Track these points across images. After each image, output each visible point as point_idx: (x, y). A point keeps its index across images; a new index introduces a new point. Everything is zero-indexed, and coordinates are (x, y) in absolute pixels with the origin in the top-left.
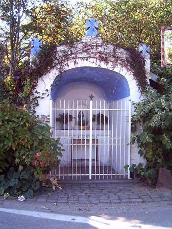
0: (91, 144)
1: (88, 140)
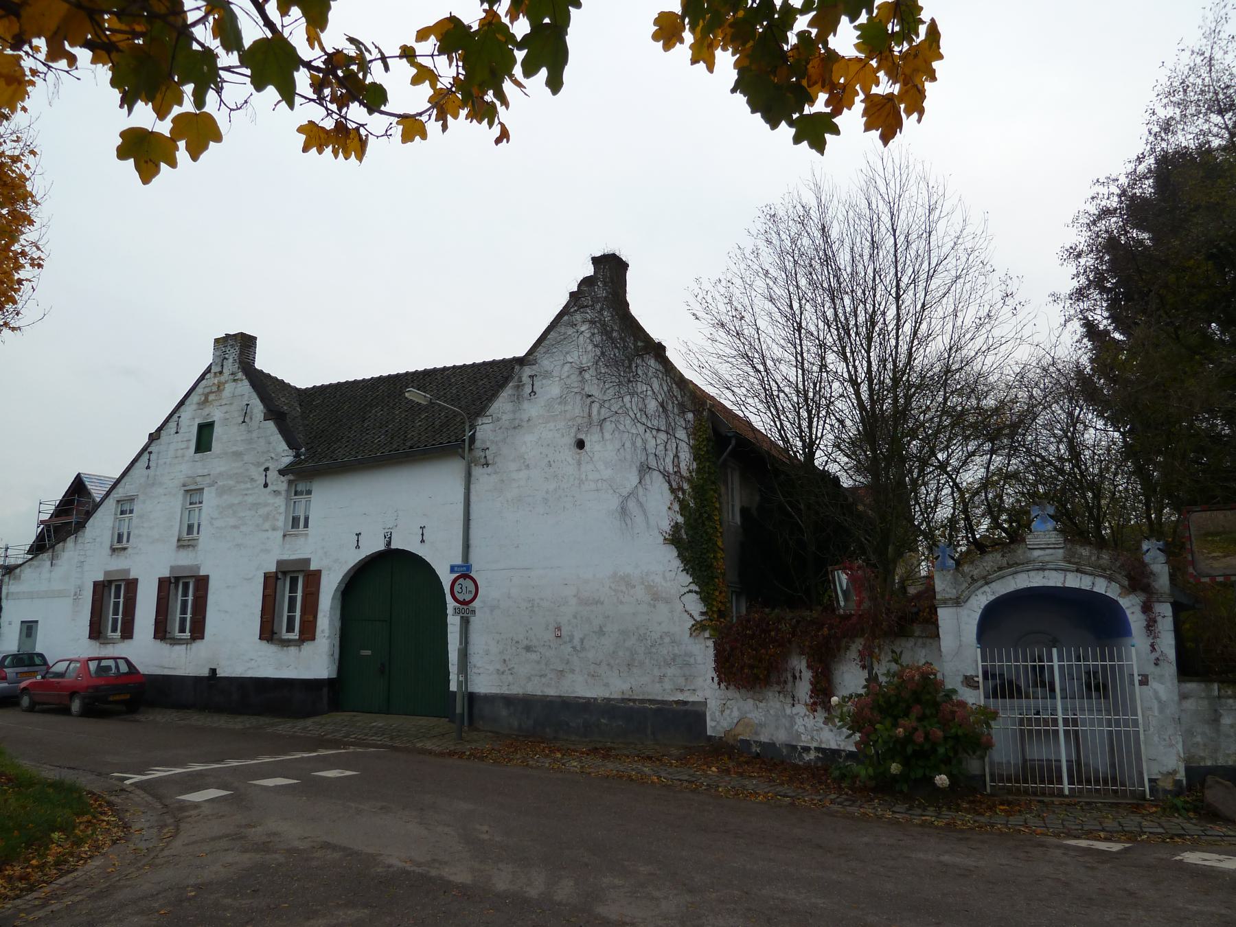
0: (1061, 728)
1: (1055, 722)
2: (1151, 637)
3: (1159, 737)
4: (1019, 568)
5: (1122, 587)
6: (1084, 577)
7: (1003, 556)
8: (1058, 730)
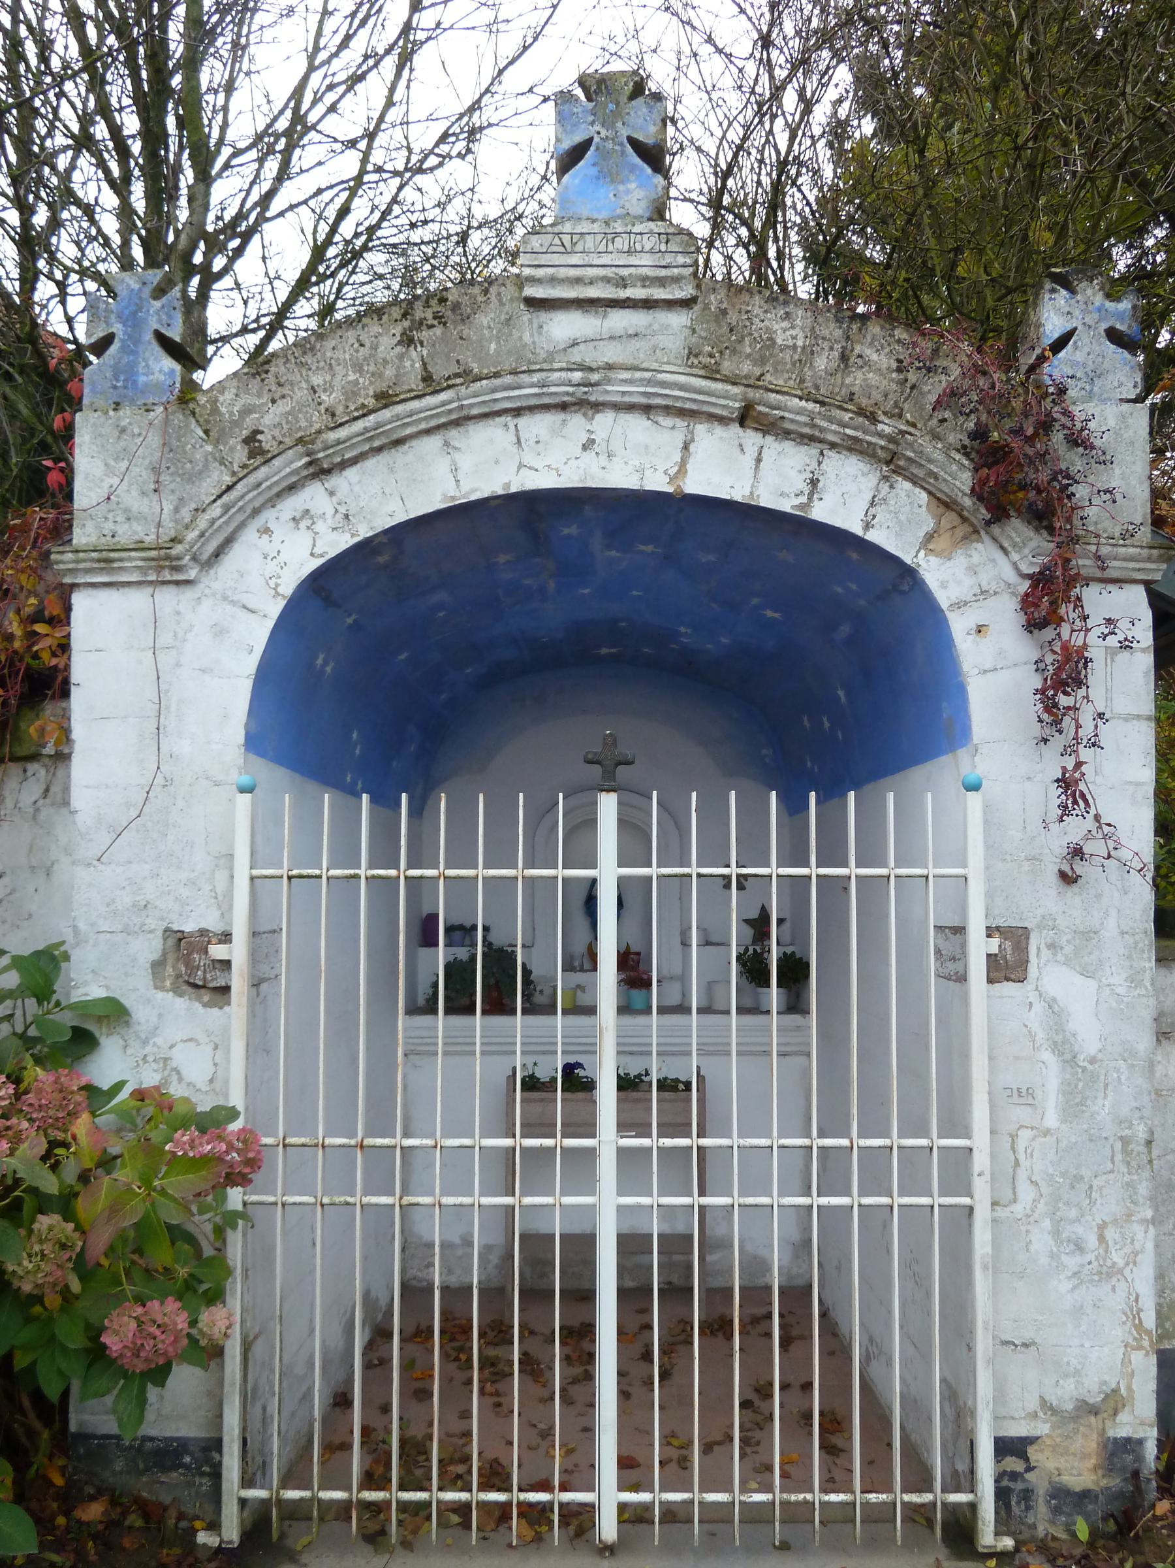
3: (1056, 1233)
4: (472, 397)
5: (944, 504)
6: (773, 447)
7: (408, 341)
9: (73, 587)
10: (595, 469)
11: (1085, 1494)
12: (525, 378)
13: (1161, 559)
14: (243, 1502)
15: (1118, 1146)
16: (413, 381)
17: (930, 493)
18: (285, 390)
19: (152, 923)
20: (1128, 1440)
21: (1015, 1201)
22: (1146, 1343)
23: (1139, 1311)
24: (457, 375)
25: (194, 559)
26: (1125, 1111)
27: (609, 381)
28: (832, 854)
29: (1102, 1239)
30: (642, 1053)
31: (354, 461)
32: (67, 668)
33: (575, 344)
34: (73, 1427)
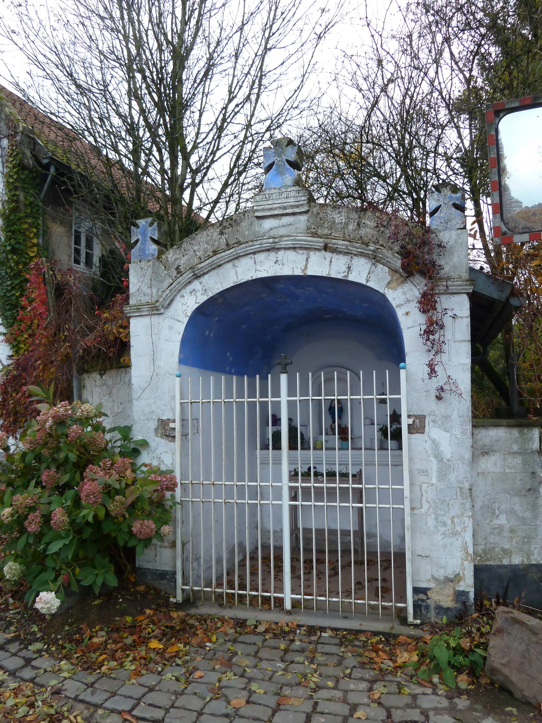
2: (433, 352)
3: (436, 519)
4: (240, 250)
7: (221, 233)
8: (281, 505)
9: (130, 317)
10: (279, 270)
11: (448, 609)
12: (255, 243)
13: (470, 285)
14: (183, 590)
15: (458, 490)
16: (224, 246)
17: (389, 268)
18: (186, 252)
19: (154, 417)
20: (463, 591)
21: (422, 508)
22: (469, 559)
23: (467, 547)
24: (236, 243)
25: (162, 307)
26: (461, 478)
27: (281, 241)
28: (264, 394)
29: (453, 522)
30: (333, 464)
31: (207, 273)
32: (129, 341)
33: (271, 229)
34: (137, 566)
